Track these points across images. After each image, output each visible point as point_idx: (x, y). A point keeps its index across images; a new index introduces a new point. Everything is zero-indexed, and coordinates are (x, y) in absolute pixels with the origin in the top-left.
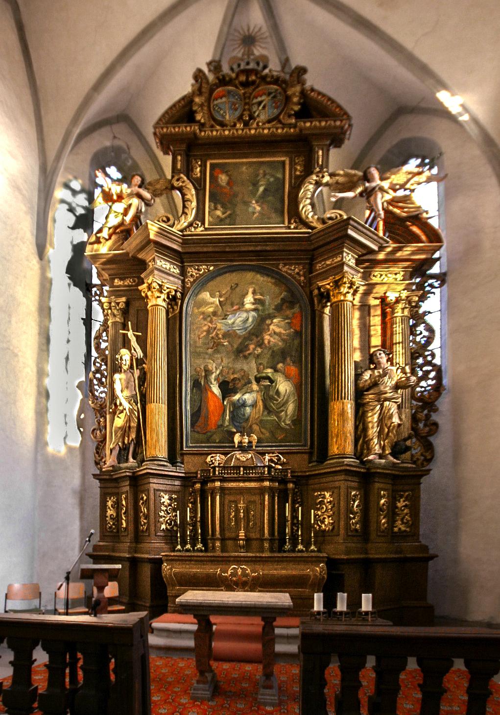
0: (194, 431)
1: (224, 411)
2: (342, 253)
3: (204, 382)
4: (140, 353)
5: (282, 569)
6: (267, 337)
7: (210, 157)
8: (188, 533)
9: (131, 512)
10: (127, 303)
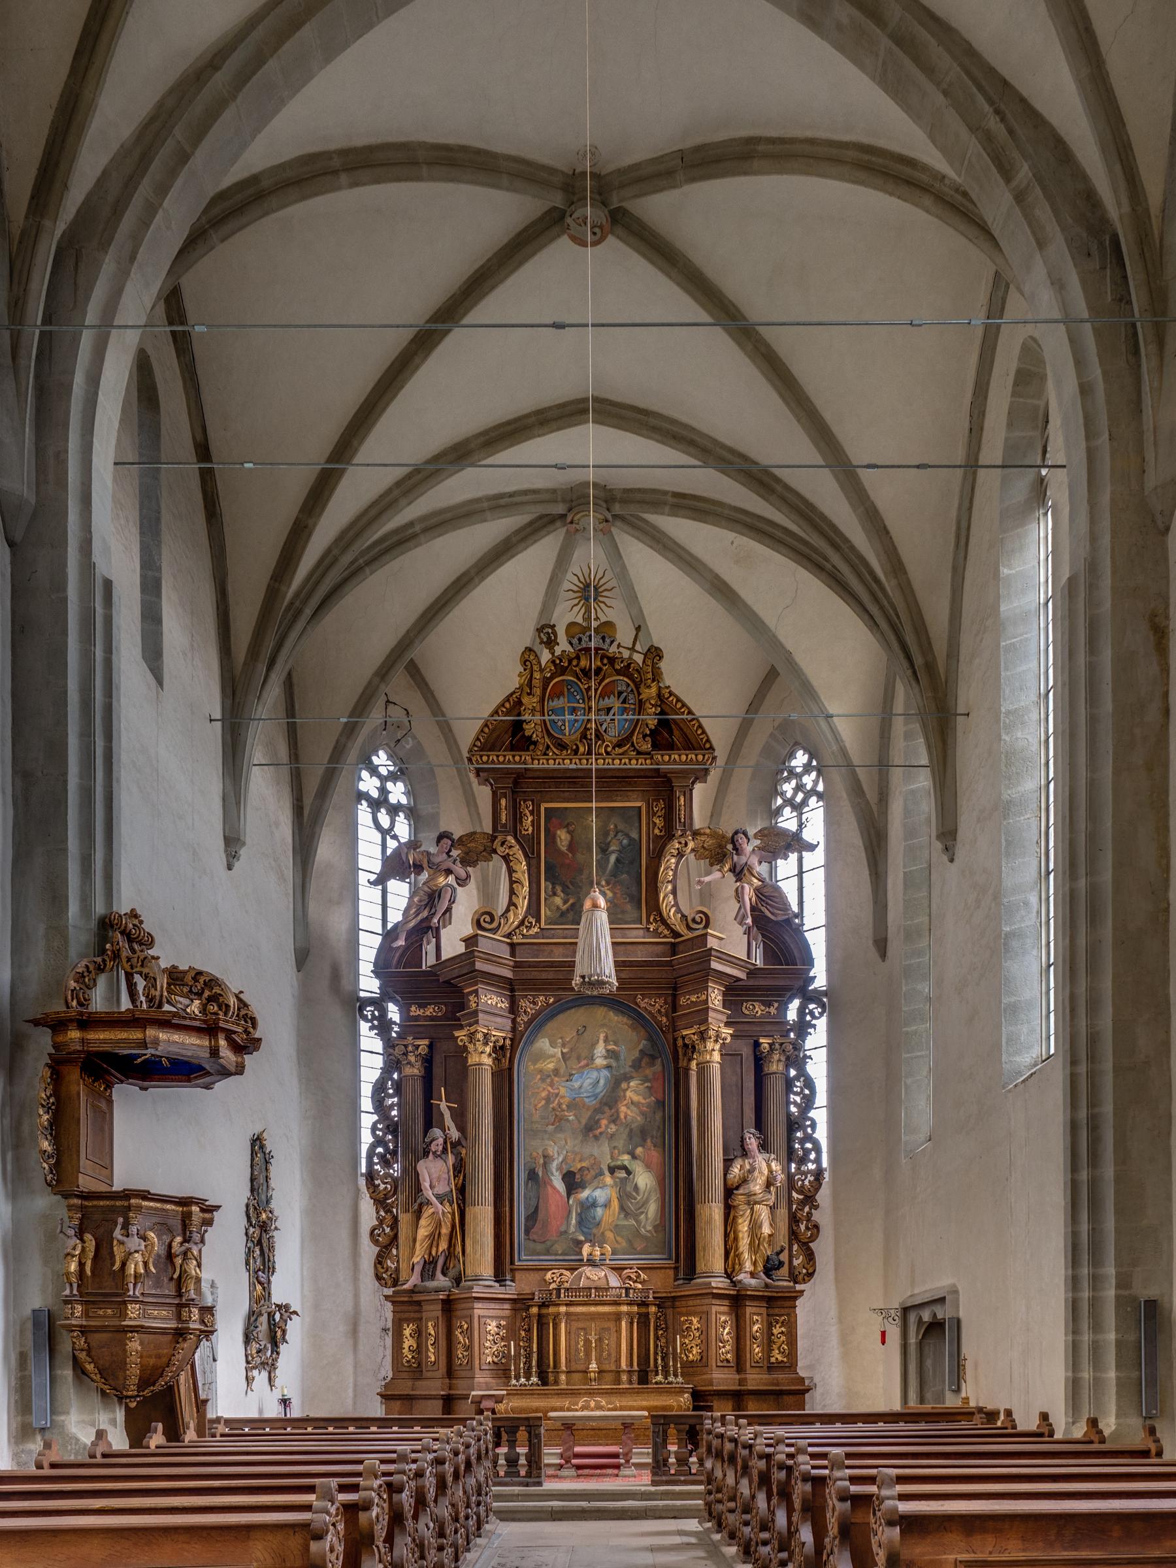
1: (570, 1212)
2: (706, 988)
4: (455, 1134)
5: (645, 1400)
6: (623, 1109)
8: (522, 1365)
9: (443, 1342)
10: (430, 1046)
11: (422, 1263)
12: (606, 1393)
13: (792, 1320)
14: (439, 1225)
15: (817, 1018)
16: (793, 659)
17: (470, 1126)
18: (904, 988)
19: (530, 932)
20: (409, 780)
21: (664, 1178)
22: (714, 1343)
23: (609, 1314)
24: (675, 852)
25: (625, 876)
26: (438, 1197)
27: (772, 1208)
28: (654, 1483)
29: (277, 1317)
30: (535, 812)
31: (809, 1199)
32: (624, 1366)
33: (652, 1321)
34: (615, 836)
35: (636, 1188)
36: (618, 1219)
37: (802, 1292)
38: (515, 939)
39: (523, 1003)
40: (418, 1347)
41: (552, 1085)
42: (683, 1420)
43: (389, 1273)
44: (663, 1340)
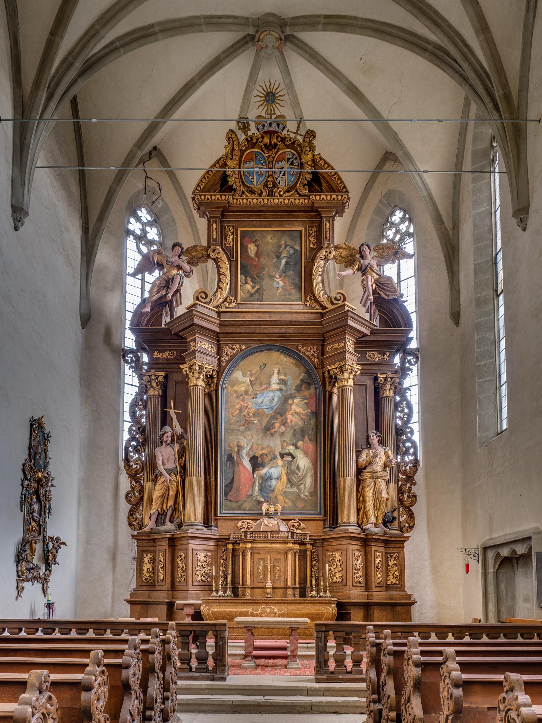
0: (227, 499)
1: (254, 482)
3: (237, 456)
5: (304, 608)
6: (289, 417)
7: (240, 223)
8: (220, 583)
10: (166, 377)
11: (156, 514)
12: (278, 603)
13: (402, 556)
14: (168, 489)
15: (413, 365)
16: (398, 138)
17: (189, 424)
18: (476, 338)
19: (231, 306)
20: (160, 227)
21: (316, 461)
22: (351, 570)
23: (280, 549)
24: (323, 257)
25: (291, 272)
26: (167, 470)
27: (388, 482)
28: (317, 680)
29: (51, 545)
30: (235, 233)
31: (410, 478)
32: (289, 584)
33: (309, 554)
34: (285, 248)
35: (298, 468)
36: (286, 487)
37: (409, 537)
38: (221, 310)
39: (226, 349)
40: (153, 569)
41: (243, 400)
42: (341, 629)
43: (137, 522)
44: (316, 568)
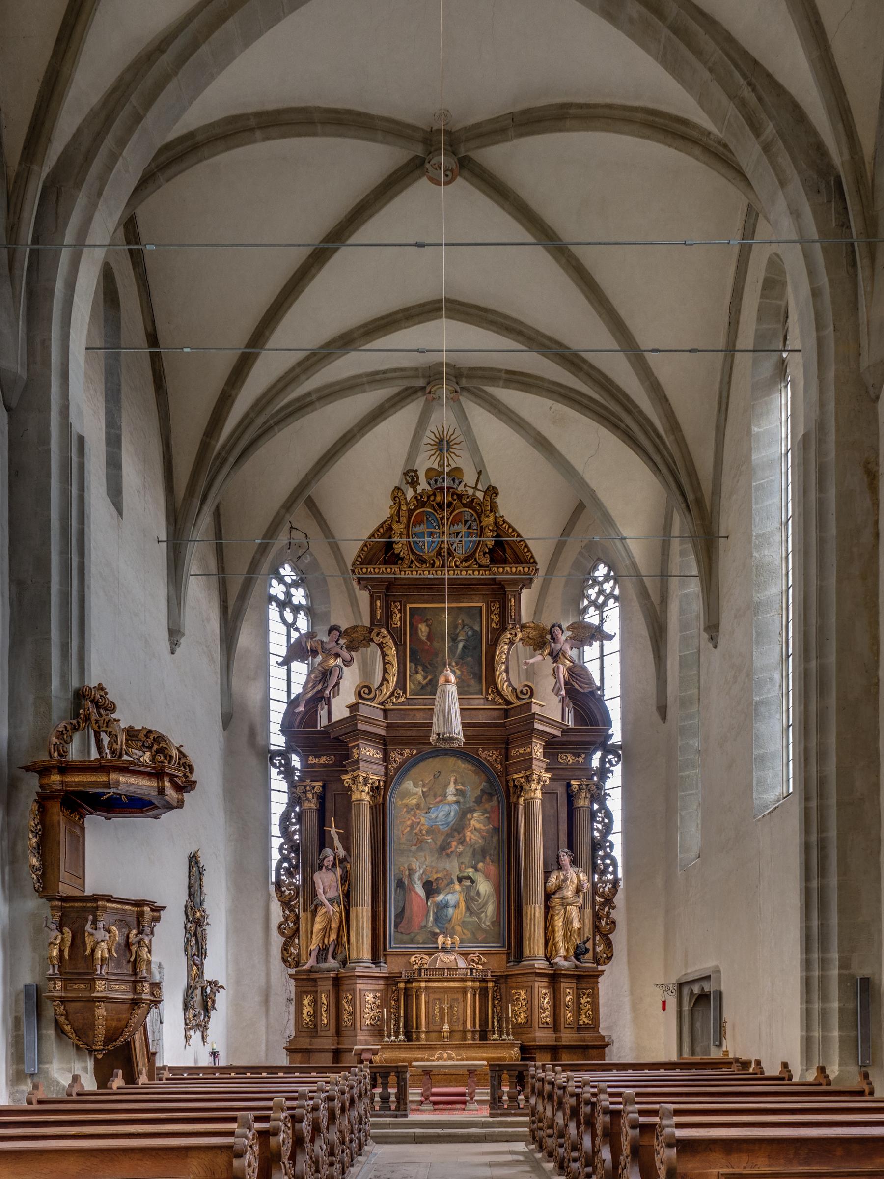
1: (428, 911)
2: (531, 743)
4: (342, 853)
5: (485, 1053)
6: (468, 834)
8: (392, 1027)
9: (333, 1009)
10: (324, 787)
11: (317, 950)
12: (456, 1048)
13: (596, 992)
14: (330, 921)
15: (614, 766)
16: (596, 495)
17: (353, 847)
18: (679, 743)
19: (399, 701)
20: (308, 586)
21: (499, 886)
22: (536, 1010)
23: (458, 988)
24: (508, 641)
25: (469, 659)
26: (329, 900)
27: (581, 909)
28: (492, 1115)
29: (209, 990)
30: (402, 611)
31: (608, 901)
32: (469, 1027)
33: (490, 993)
34: (463, 628)
35: (478, 893)
36: (464, 916)
37: (603, 971)
38: (387, 706)
39: (393, 754)
40: (314, 1013)
41: (415, 815)
42: (513, 1068)
43: (292, 957)
44: (499, 1008)
